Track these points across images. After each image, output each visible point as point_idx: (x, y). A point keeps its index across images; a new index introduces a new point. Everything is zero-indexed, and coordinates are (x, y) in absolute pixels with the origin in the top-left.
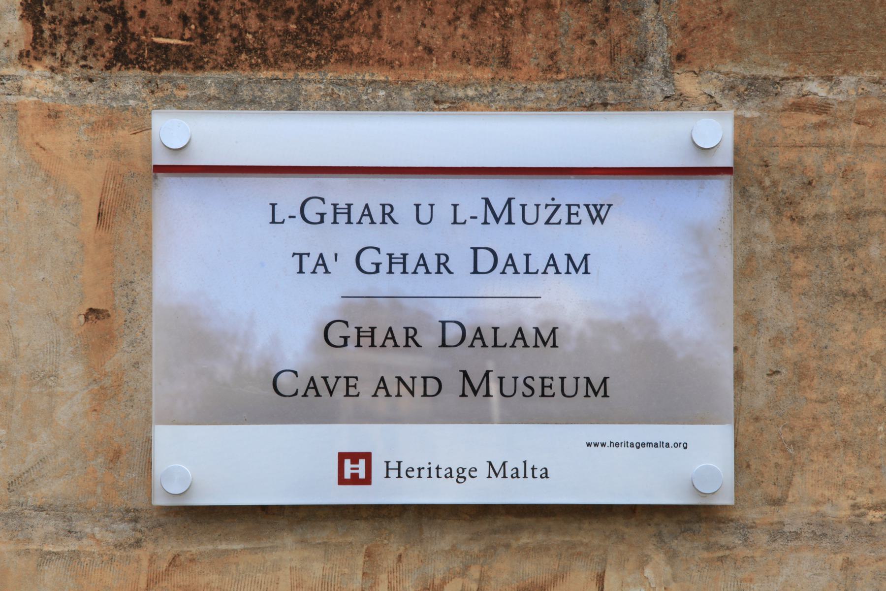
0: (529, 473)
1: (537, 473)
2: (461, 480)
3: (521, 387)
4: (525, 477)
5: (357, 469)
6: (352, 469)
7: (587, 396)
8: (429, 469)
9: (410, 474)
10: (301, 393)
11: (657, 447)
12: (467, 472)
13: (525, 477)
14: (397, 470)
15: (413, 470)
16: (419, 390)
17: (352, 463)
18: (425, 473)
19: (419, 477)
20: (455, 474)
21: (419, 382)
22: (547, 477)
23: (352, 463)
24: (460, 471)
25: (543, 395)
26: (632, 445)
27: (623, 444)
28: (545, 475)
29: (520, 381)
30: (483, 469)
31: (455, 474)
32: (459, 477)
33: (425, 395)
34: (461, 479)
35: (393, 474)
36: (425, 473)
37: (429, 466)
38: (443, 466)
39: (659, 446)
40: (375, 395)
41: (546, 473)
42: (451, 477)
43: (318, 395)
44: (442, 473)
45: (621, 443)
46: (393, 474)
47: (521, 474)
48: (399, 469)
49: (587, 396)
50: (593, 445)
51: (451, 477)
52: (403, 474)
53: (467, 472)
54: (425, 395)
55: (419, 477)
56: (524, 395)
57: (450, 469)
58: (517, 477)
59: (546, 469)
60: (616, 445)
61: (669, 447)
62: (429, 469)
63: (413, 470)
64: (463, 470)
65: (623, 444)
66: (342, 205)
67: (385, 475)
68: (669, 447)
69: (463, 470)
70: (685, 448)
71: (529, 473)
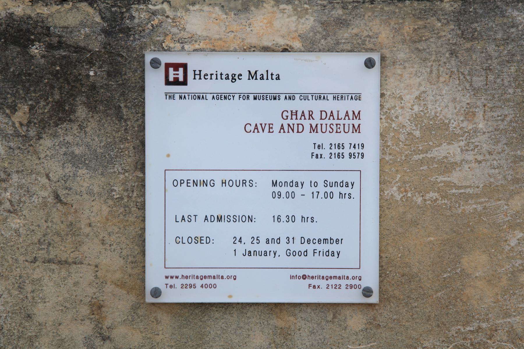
0: (219, 76)
1: (274, 77)
2: (234, 81)
3: (329, 129)
4: (267, 79)
5: (174, 74)
6: (174, 74)
7: (353, 132)
8: (217, 75)
9: (206, 77)
10: (252, 131)
11: (340, 279)
12: (237, 76)
13: (267, 79)
14: (198, 74)
15: (207, 75)
16: (296, 130)
17: (174, 70)
18: (214, 77)
19: (211, 79)
20: (230, 77)
21: (296, 126)
22: (279, 79)
23: (174, 70)
24: (233, 76)
25: (337, 132)
26: (323, 277)
27: (317, 278)
28: (278, 78)
29: (328, 126)
30: (246, 75)
31: (230, 77)
32: (233, 79)
33: (298, 132)
34: (234, 80)
35: (197, 77)
36: (214, 77)
37: (216, 73)
38: (224, 73)
39: (341, 278)
40: (280, 132)
41: (279, 77)
42: (228, 79)
43: (258, 132)
44: (224, 77)
45: (316, 276)
46: (197, 77)
47: (265, 77)
48: (200, 75)
49: (353, 132)
50: (169, 278)
51: (228, 79)
52: (202, 77)
53: (237, 76)
54: (298, 132)
55: (211, 79)
56: (330, 132)
57: (228, 74)
58: (263, 79)
59: (279, 75)
60: (312, 277)
61: (223, 279)
62: (217, 75)
63: (207, 75)
64: (235, 75)
65: (317, 278)
66: (294, 111)
67: (193, 78)
68: (223, 279)
69: (235, 75)
70: (235, 279)
71: (219, 76)
